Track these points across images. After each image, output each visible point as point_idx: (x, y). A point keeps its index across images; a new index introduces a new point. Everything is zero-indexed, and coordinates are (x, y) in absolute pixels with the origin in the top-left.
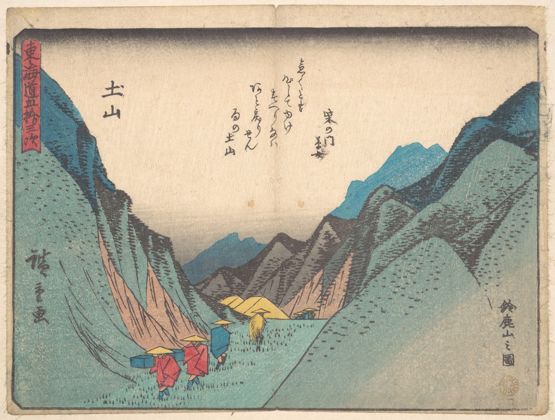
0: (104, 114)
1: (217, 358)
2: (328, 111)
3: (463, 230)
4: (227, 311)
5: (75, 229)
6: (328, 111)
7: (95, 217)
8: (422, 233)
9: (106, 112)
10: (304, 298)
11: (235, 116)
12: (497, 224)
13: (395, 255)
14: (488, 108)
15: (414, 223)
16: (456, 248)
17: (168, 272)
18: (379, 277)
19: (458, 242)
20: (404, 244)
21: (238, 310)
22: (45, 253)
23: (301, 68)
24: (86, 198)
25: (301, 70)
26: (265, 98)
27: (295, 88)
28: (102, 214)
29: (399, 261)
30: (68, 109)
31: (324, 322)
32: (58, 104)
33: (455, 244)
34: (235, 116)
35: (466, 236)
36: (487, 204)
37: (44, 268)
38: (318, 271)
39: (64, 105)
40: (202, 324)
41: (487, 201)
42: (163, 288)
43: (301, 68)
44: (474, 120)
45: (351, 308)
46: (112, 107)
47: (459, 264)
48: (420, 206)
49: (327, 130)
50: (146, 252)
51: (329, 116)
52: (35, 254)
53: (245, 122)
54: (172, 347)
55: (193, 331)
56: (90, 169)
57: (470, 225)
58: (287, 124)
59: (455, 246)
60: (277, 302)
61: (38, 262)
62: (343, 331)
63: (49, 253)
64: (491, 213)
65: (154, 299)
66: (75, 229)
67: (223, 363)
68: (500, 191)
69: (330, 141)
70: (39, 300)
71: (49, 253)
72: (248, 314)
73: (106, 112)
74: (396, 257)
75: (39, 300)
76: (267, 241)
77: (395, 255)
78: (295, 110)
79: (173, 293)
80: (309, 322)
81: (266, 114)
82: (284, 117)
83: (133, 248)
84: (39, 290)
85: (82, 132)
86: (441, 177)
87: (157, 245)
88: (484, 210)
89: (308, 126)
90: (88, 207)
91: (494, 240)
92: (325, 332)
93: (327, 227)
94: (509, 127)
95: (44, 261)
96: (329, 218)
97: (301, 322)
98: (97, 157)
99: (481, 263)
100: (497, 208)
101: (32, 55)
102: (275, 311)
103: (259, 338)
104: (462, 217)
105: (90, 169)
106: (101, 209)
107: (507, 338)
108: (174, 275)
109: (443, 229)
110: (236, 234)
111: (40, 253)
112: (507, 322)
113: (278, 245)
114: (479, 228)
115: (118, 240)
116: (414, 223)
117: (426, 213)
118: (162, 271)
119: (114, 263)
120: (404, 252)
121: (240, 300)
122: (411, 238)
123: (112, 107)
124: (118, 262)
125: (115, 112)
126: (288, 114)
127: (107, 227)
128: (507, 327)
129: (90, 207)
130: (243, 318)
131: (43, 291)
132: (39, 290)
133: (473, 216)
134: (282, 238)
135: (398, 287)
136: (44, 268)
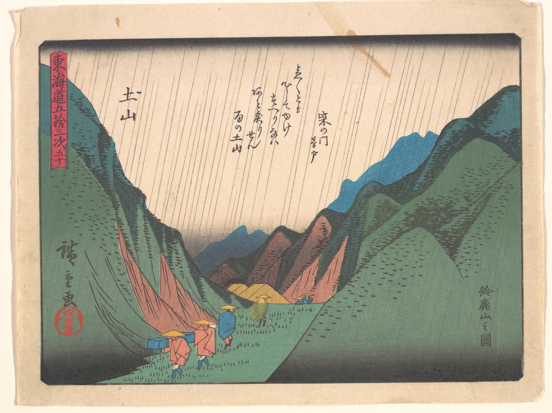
0: (121, 117)
1: (224, 340)
2: (322, 113)
3: (444, 222)
4: (232, 297)
5: (97, 222)
6: (322, 113)
7: (114, 212)
8: (407, 225)
9: (123, 116)
10: (302, 287)
11: (239, 117)
12: (476, 216)
13: (383, 244)
14: (466, 111)
15: (400, 216)
16: (438, 238)
17: (179, 261)
18: (369, 264)
19: (439, 232)
20: (392, 234)
21: (243, 296)
22: (73, 244)
23: (298, 73)
24: (107, 194)
25: (297, 75)
26: (267, 103)
27: (292, 90)
28: (121, 209)
29: (386, 250)
30: (90, 113)
31: (322, 305)
32: (81, 109)
33: (436, 234)
34: (239, 117)
35: (446, 227)
36: (467, 198)
37: (72, 256)
38: (317, 256)
39: (86, 110)
40: (210, 308)
41: (467, 195)
42: (175, 276)
43: (298, 73)
44: (454, 121)
45: (344, 292)
46: (128, 111)
47: (442, 253)
48: (404, 199)
49: (321, 131)
50: (160, 243)
51: (323, 118)
52: (65, 244)
53: (249, 125)
54: (185, 330)
55: (202, 315)
56: (110, 168)
57: (451, 216)
58: (286, 125)
59: (437, 236)
60: (279, 287)
61: (68, 252)
62: (337, 315)
63: (76, 244)
64: (471, 205)
65: (139, 299)
66: (97, 222)
67: (229, 345)
68: (479, 185)
69: (324, 141)
70: (68, 286)
71: (76, 244)
72: (252, 299)
73: (123, 116)
74: (385, 246)
75: (68, 286)
76: (270, 232)
77: (383, 244)
78: (292, 112)
79: (184, 282)
80: (307, 306)
81: (266, 117)
82: (283, 119)
83: (148, 239)
84: (69, 278)
85: (103, 132)
86: (424, 174)
87: (167, 236)
88: (464, 203)
89: (304, 126)
90: (109, 203)
91: (473, 230)
92: (322, 315)
93: (324, 219)
94: (486, 127)
95: (72, 251)
96: (324, 212)
97: (300, 307)
98: (115, 156)
99: (461, 251)
100: (476, 201)
101: (59, 64)
102: (276, 298)
103: (262, 321)
104: (444, 210)
105: (110, 168)
106: (120, 204)
107: (484, 320)
108: (185, 263)
109: (422, 220)
110: (243, 228)
111: (69, 244)
112: (485, 305)
113: (280, 234)
114: (461, 218)
115: (134, 233)
116: (400, 216)
117: (411, 207)
118: (174, 260)
119: (131, 253)
120: (392, 242)
121: (244, 287)
122: (397, 229)
123: (128, 111)
124: (135, 254)
125: (131, 115)
126: (287, 116)
127: (125, 221)
128: (485, 310)
129: (111, 203)
130: (247, 303)
131: (72, 278)
132: (69, 278)
133: (454, 208)
134: (282, 229)
135: (387, 273)
136: (72, 256)
